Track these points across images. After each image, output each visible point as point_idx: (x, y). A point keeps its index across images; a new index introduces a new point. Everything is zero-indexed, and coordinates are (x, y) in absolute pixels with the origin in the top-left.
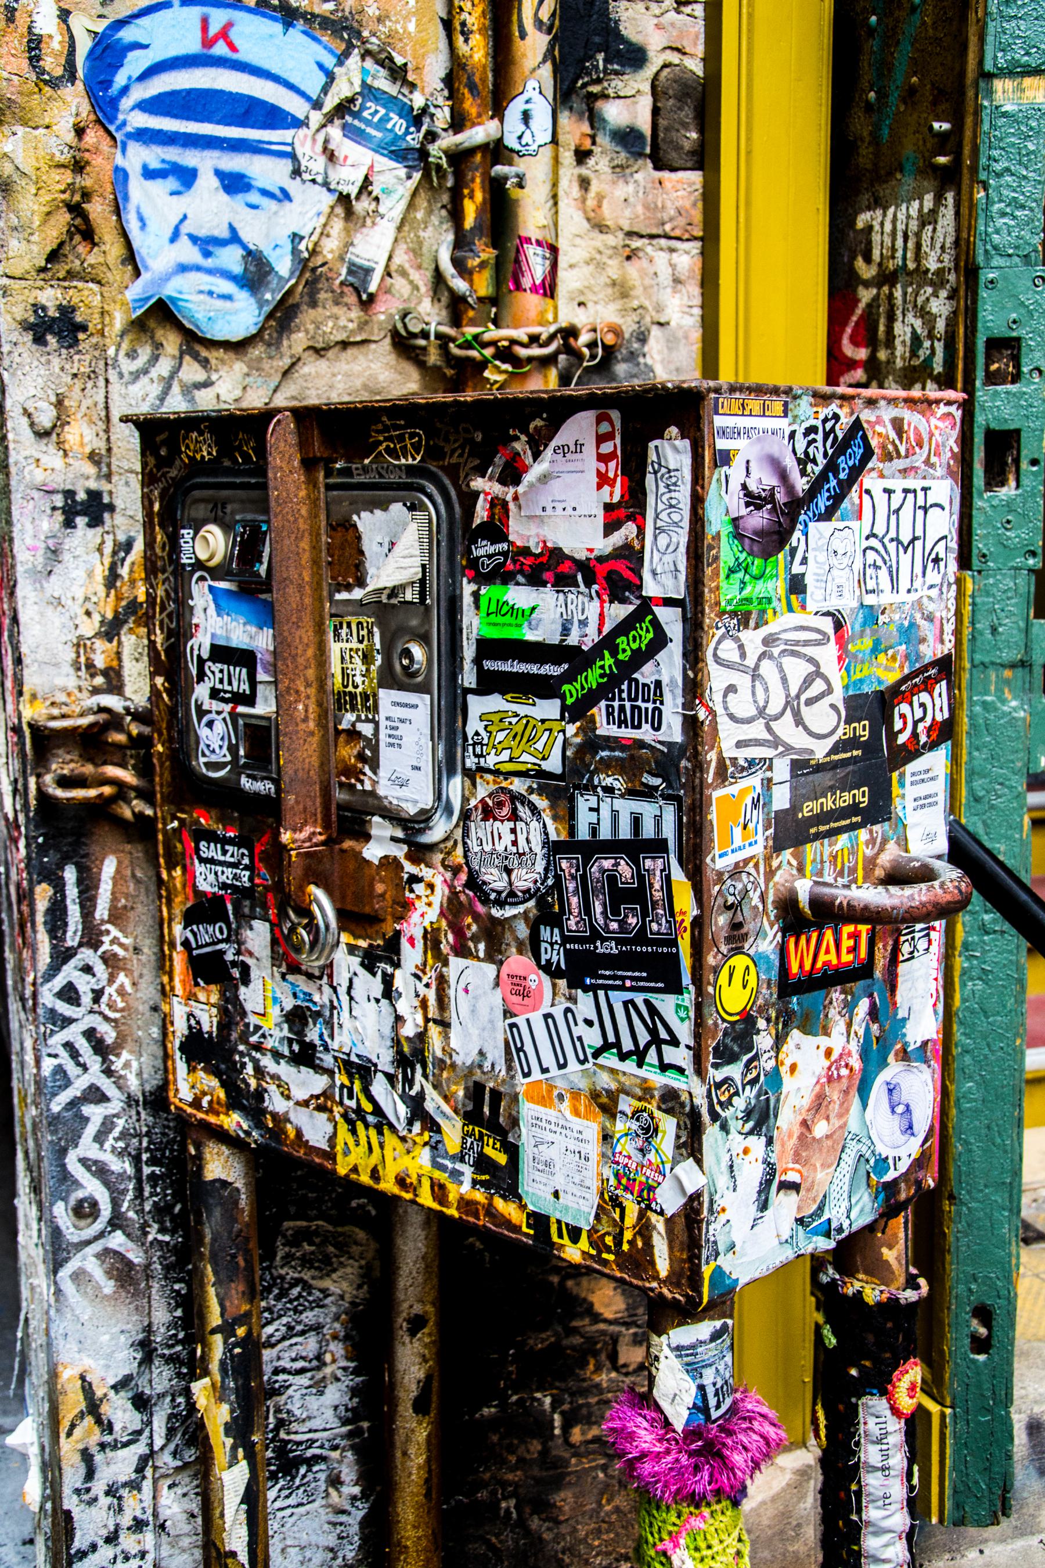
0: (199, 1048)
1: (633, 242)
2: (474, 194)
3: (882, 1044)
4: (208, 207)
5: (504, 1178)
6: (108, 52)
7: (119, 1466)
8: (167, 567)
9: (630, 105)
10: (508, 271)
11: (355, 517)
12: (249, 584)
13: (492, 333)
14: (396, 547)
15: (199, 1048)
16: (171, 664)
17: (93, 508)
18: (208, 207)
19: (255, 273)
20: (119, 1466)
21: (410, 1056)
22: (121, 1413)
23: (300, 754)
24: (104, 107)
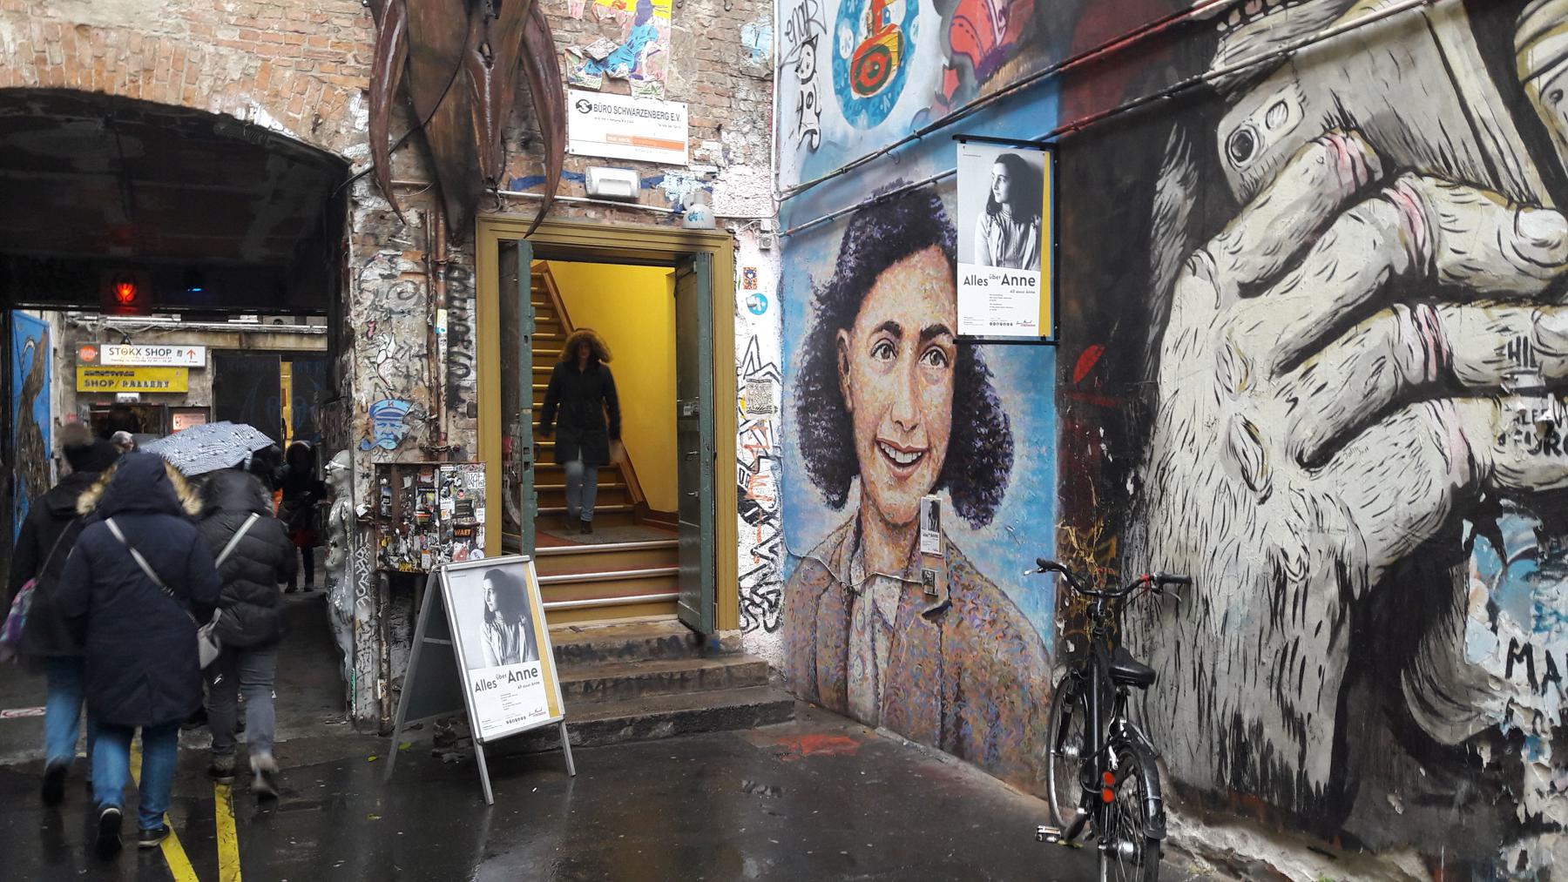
0: (381, 558)
1: (463, 430)
2: (433, 425)
3: (474, 546)
4: (388, 429)
5: (419, 565)
6: (373, 408)
7: (366, 637)
8: (378, 485)
9: (463, 409)
10: (439, 437)
11: (1538, 523)
12: (389, 488)
13: (762, 333)
14: (408, 482)
15: (381, 558)
16: (378, 500)
17: (368, 476)
18: (388, 429)
19: (396, 439)
20: (366, 637)
21: (409, 551)
22: (366, 628)
23: (395, 511)
24: (372, 415)
